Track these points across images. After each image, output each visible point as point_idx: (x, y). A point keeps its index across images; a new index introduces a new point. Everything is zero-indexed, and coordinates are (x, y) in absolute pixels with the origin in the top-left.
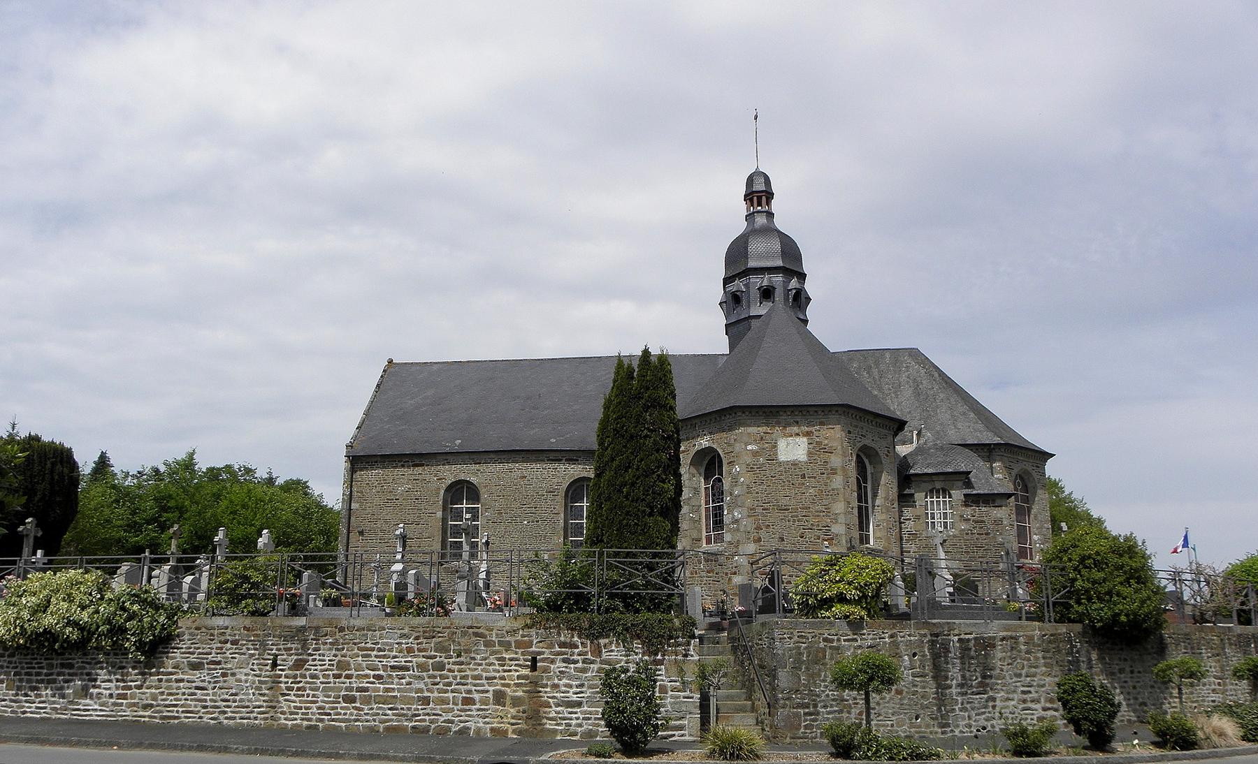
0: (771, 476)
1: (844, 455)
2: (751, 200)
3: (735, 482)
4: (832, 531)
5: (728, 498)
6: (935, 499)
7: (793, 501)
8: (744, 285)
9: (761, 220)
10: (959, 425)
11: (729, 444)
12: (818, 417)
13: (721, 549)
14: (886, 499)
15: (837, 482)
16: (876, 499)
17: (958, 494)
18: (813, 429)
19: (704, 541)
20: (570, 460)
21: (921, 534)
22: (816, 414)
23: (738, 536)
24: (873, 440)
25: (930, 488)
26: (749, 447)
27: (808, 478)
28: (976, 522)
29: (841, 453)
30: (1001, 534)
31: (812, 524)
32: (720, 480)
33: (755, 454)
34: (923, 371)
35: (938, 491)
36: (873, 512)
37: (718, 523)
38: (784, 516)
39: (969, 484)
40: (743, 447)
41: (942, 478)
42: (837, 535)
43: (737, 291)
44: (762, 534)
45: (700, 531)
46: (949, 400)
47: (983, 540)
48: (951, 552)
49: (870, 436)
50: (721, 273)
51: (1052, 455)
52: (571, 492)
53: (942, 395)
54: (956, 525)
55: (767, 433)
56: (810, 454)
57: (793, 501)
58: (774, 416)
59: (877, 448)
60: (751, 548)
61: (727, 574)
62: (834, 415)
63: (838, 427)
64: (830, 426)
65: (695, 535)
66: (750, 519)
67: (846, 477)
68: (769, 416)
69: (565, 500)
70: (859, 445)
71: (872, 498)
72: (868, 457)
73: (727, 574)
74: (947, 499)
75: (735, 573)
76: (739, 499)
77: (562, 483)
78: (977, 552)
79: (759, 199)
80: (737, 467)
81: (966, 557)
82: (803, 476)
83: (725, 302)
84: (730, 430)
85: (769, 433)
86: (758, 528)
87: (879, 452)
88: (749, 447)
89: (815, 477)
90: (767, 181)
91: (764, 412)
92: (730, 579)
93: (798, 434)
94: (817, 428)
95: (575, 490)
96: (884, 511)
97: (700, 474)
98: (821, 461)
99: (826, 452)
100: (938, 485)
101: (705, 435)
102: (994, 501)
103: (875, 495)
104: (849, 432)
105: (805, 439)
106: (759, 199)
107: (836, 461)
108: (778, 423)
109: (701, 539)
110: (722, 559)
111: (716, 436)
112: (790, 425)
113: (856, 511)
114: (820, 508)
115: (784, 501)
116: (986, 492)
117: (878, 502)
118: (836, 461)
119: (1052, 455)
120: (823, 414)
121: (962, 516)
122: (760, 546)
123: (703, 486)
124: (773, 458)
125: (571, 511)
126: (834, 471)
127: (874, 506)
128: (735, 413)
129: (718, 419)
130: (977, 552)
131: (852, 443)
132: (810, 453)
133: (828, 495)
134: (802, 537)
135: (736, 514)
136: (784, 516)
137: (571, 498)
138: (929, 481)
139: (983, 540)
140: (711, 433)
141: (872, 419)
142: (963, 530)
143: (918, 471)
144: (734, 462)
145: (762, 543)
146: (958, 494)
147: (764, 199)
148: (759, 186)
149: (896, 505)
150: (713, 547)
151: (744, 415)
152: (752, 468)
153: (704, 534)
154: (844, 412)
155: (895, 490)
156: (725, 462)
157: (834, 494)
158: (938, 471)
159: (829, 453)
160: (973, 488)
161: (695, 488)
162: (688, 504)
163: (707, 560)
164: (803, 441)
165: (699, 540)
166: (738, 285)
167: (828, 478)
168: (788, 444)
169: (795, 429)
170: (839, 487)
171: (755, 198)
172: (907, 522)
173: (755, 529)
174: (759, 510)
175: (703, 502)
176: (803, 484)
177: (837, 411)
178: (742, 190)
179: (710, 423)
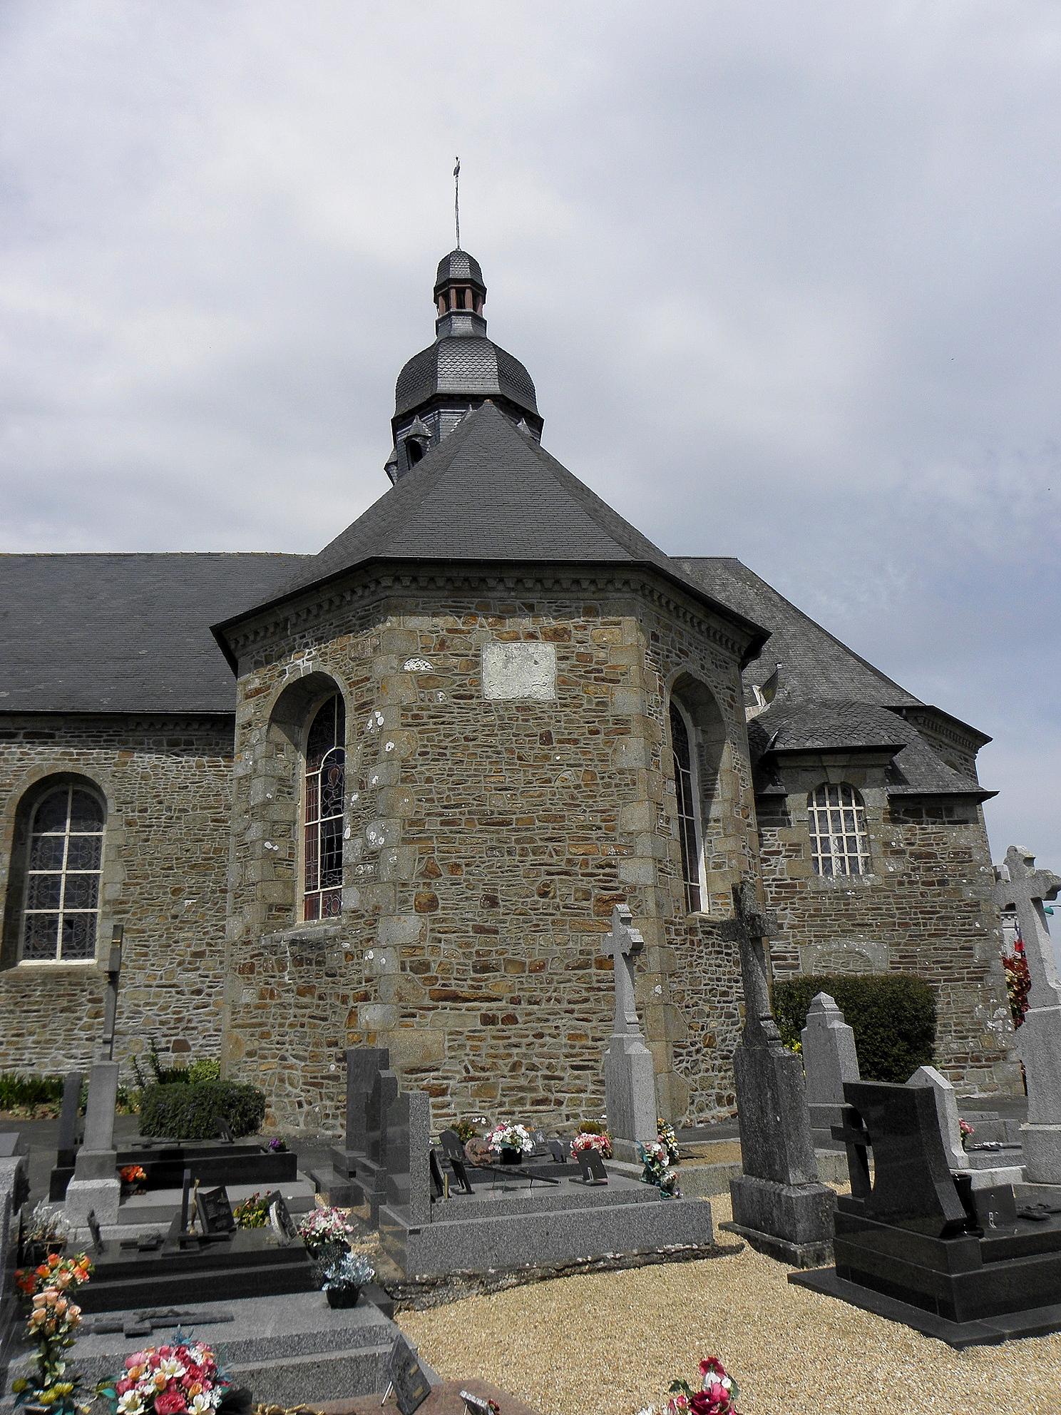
0: (466, 739)
1: (645, 687)
2: (446, 297)
3: (373, 754)
4: (622, 876)
5: (355, 797)
6: (828, 808)
7: (521, 801)
8: (429, 427)
9: (462, 325)
10: (834, 676)
11: (360, 661)
12: (580, 595)
13: (332, 931)
14: (734, 802)
15: (631, 752)
16: (710, 803)
17: (876, 797)
18: (569, 624)
19: (300, 911)
20: (35, 737)
21: (804, 885)
22: (574, 588)
23: (379, 894)
24: (703, 667)
25: (818, 783)
26: (410, 666)
27: (560, 742)
28: (918, 856)
29: (638, 681)
30: (970, 882)
31: (569, 861)
32: (339, 756)
33: (424, 681)
34: (752, 592)
35: (833, 790)
36: (705, 834)
37: (333, 865)
38: (499, 841)
39: (895, 776)
40: (395, 663)
41: (842, 760)
42: (634, 888)
43: (416, 436)
44: (442, 888)
45: (290, 885)
46: (806, 635)
47: (935, 897)
48: (871, 925)
49: (695, 655)
50: (391, 412)
51: (988, 740)
52: (36, 806)
53: (792, 629)
54: (877, 863)
55: (456, 631)
56: (562, 683)
57: (521, 801)
58: (473, 589)
59: (711, 685)
60: (409, 926)
61: (344, 1000)
62: (619, 590)
63: (629, 622)
64: (612, 618)
65: (276, 895)
66: (408, 850)
67: (652, 742)
68: (459, 589)
69: (16, 823)
70: (676, 672)
71: (702, 802)
72: (692, 707)
73: (344, 1000)
74: (854, 808)
75: (365, 998)
76: (381, 796)
77: (11, 785)
78: (925, 925)
79: (460, 293)
80: (378, 714)
81: (902, 936)
82: (547, 739)
83: (395, 463)
84: (363, 626)
85: (461, 632)
86: (430, 873)
87: (717, 696)
88: (410, 666)
89: (576, 741)
90: (474, 265)
91: (449, 580)
92: (353, 1014)
93: (532, 636)
94: (580, 621)
95: (46, 802)
96: (731, 830)
97: (297, 746)
98: (589, 701)
99: (603, 680)
100: (835, 777)
101: (306, 645)
102: (950, 812)
103: (708, 795)
104: (655, 637)
105: (550, 648)
106: (460, 293)
107: (627, 700)
108: (485, 609)
109: (293, 905)
110: (334, 959)
111: (332, 645)
112: (512, 612)
113: (674, 828)
114: (588, 818)
115: (498, 802)
116: (934, 790)
117: (716, 810)
118: (627, 700)
119: (988, 740)
120: (593, 588)
121: (887, 844)
122: (434, 921)
123: (303, 773)
124: (468, 693)
125: (34, 849)
126: (622, 728)
127: (706, 821)
128: (378, 582)
129: (337, 602)
130: (925, 925)
131: (664, 670)
132: (564, 682)
133: (608, 786)
134: (544, 895)
135: (372, 836)
136: (499, 841)
137: (37, 821)
138: (813, 769)
139: (935, 897)
140: (319, 640)
141: (700, 616)
142: (892, 875)
143: (793, 745)
144: (372, 702)
145: (439, 911)
146: (876, 797)
147: (469, 294)
148: (460, 271)
149: (753, 819)
150: (320, 926)
151: (397, 586)
152: (415, 717)
153: (301, 892)
154: (643, 587)
155: (749, 784)
156: (350, 705)
157: (624, 782)
158: (835, 745)
159: (611, 681)
160: (904, 782)
161: (281, 779)
162: (263, 816)
163: (298, 961)
164: (546, 652)
165: (287, 908)
166: (420, 426)
167: (608, 743)
168: (508, 659)
169: (527, 623)
170: (634, 764)
171: (453, 292)
172: (773, 860)
173: (422, 875)
174: (434, 825)
175: (301, 812)
176: (547, 757)
177: (626, 583)
178: (433, 281)
179: (317, 616)
